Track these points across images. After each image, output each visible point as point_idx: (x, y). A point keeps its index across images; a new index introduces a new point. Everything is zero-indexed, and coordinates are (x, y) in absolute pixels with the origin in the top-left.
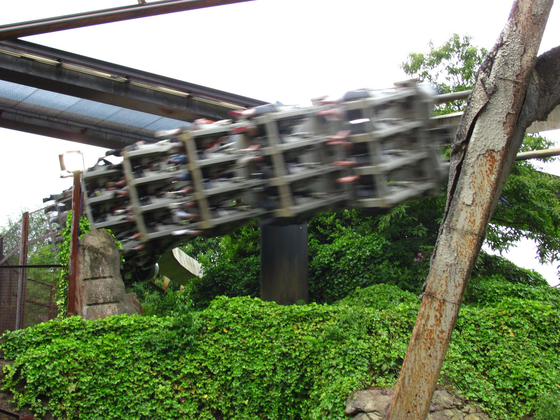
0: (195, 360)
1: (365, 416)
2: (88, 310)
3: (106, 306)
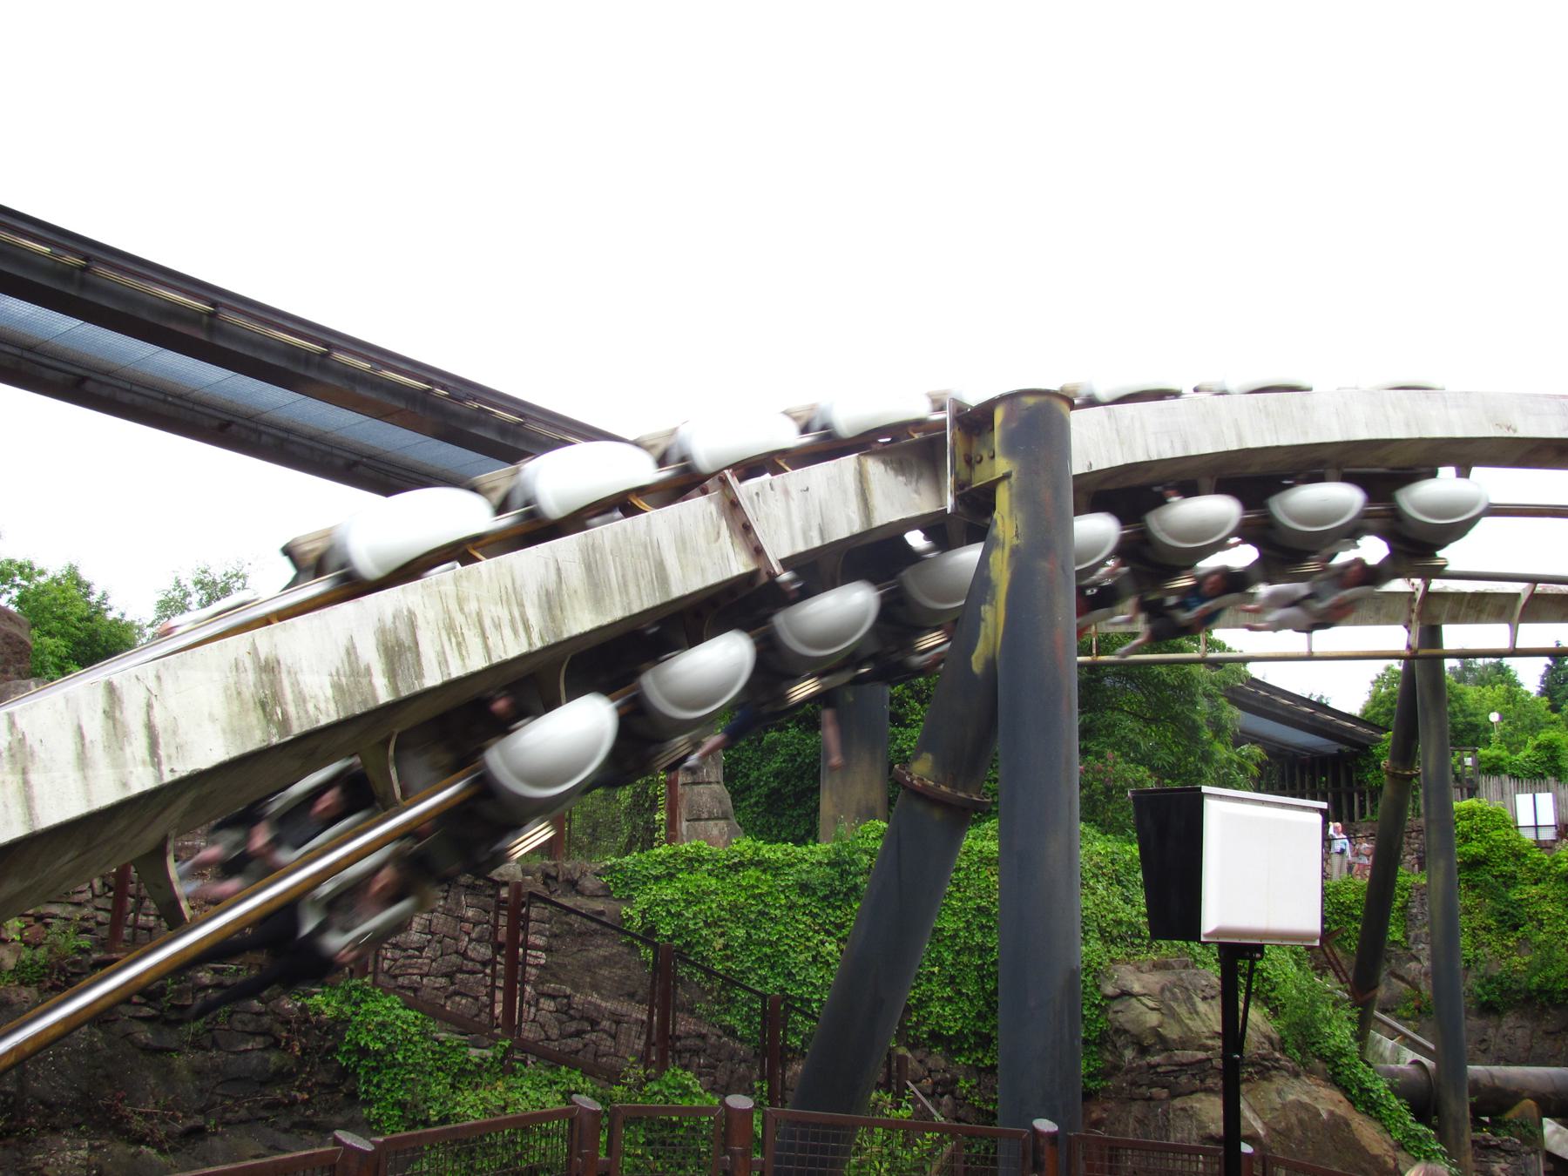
1: (1133, 1000)
3: (711, 823)
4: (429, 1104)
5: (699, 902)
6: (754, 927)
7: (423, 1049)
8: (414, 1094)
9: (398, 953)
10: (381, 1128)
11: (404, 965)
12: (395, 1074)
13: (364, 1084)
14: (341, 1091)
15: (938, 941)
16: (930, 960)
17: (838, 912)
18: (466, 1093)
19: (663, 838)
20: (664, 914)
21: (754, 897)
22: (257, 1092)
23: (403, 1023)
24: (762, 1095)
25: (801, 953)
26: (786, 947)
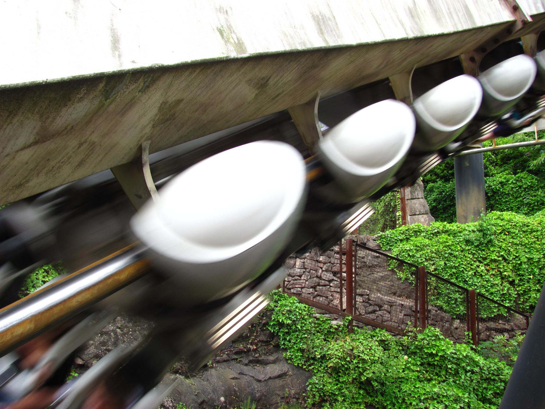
0: (495, 251)
2: (410, 218)
4: (315, 349)
5: (422, 250)
6: (447, 260)
7: (309, 322)
8: (308, 345)
9: (290, 278)
10: (292, 362)
11: (293, 284)
12: (297, 335)
13: (283, 340)
14: (271, 344)
15: (531, 264)
16: (528, 273)
17: (484, 252)
18: (332, 343)
19: (401, 223)
20: (407, 256)
21: (445, 246)
22: (231, 346)
23: (299, 310)
24: (469, 338)
25: (469, 271)
26: (463, 269)
